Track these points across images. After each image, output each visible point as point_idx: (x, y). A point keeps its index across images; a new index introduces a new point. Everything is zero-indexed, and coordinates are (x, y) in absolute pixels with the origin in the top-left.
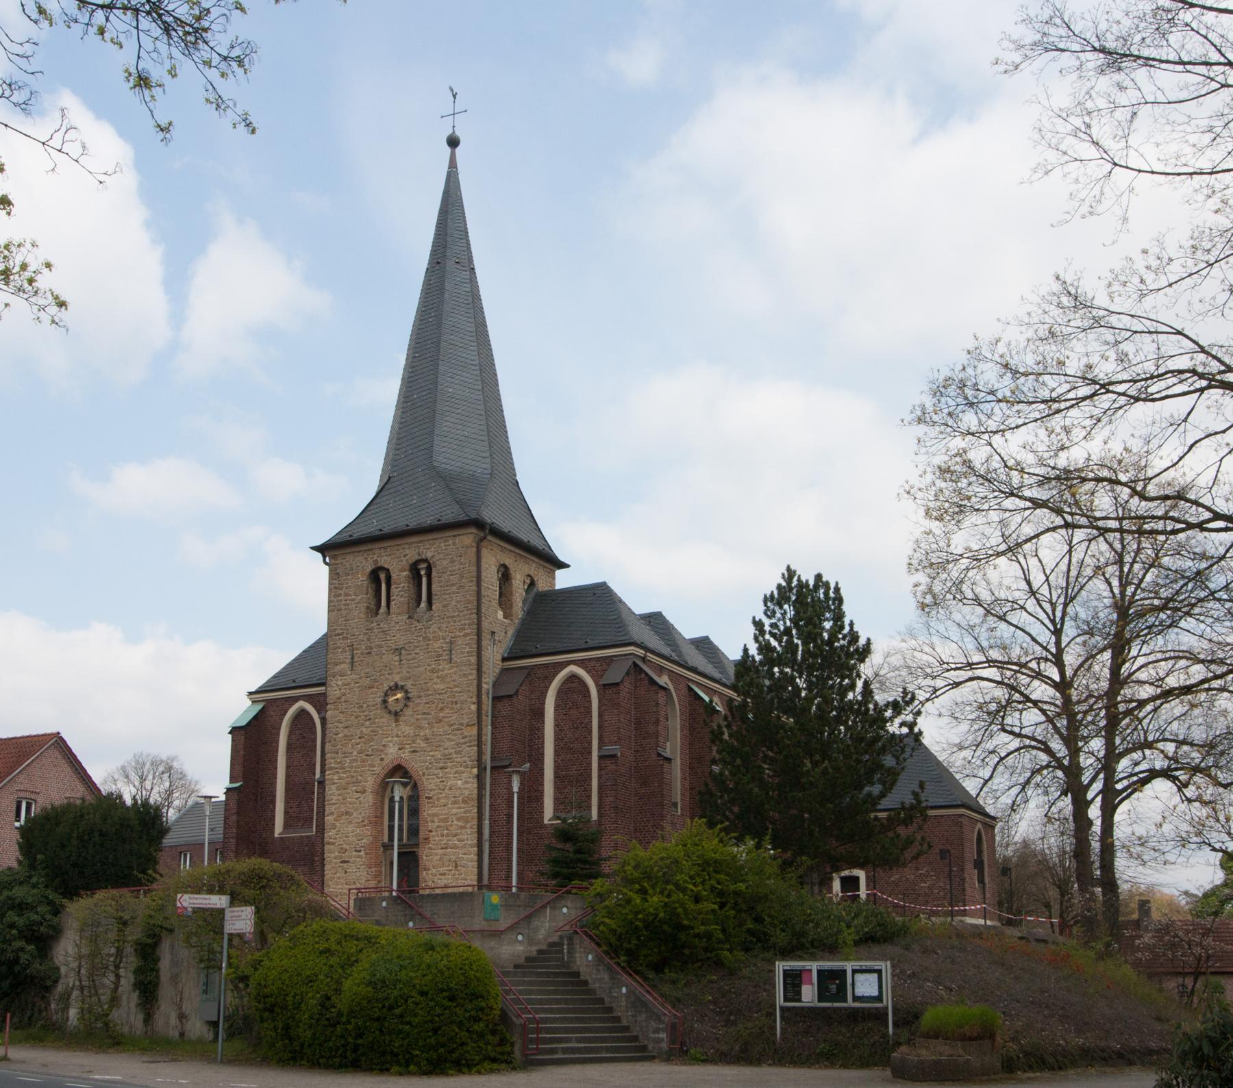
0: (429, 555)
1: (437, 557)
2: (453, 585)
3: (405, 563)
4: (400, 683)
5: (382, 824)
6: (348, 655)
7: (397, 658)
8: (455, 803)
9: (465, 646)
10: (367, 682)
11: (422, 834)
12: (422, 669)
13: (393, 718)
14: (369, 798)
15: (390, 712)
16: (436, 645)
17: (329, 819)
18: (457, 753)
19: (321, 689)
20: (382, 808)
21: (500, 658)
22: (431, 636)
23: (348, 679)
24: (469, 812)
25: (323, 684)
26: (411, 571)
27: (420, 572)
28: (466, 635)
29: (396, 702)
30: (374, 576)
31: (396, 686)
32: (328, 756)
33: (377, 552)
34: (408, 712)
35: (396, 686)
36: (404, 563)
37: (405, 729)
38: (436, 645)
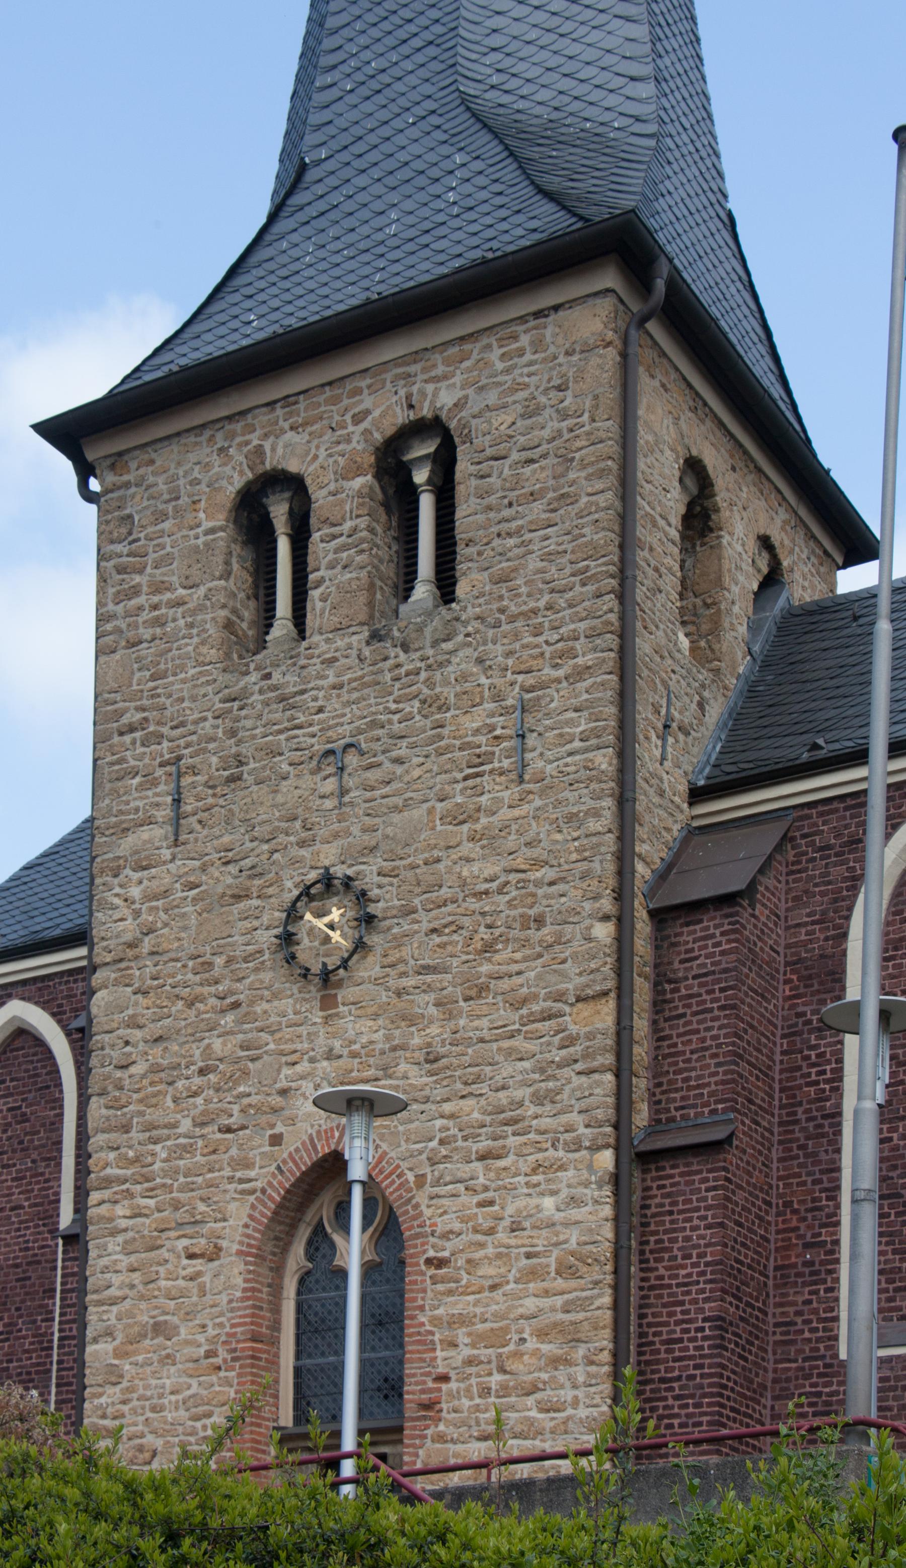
0: (446, 399)
1: (476, 404)
2: (533, 496)
3: (360, 442)
4: (339, 871)
5: (274, 1363)
6: (163, 793)
7: (330, 785)
8: (532, 1274)
9: (575, 712)
10: (226, 879)
11: (412, 1392)
12: (418, 813)
13: (314, 991)
14: (233, 1275)
15: (306, 973)
16: (471, 723)
17: (98, 1352)
18: (538, 1099)
19: (83, 951)
20: (276, 1310)
21: (683, 788)
22: (449, 693)
23: (163, 877)
24: (582, 1304)
25: (79, 937)
26: (379, 475)
27: (416, 473)
28: (580, 673)
29: (326, 932)
30: (250, 515)
31: (327, 880)
32: (97, 1140)
33: (262, 418)
34: (368, 968)
35: (327, 880)
36: (357, 444)
37: (359, 1028)
38: (471, 723)
